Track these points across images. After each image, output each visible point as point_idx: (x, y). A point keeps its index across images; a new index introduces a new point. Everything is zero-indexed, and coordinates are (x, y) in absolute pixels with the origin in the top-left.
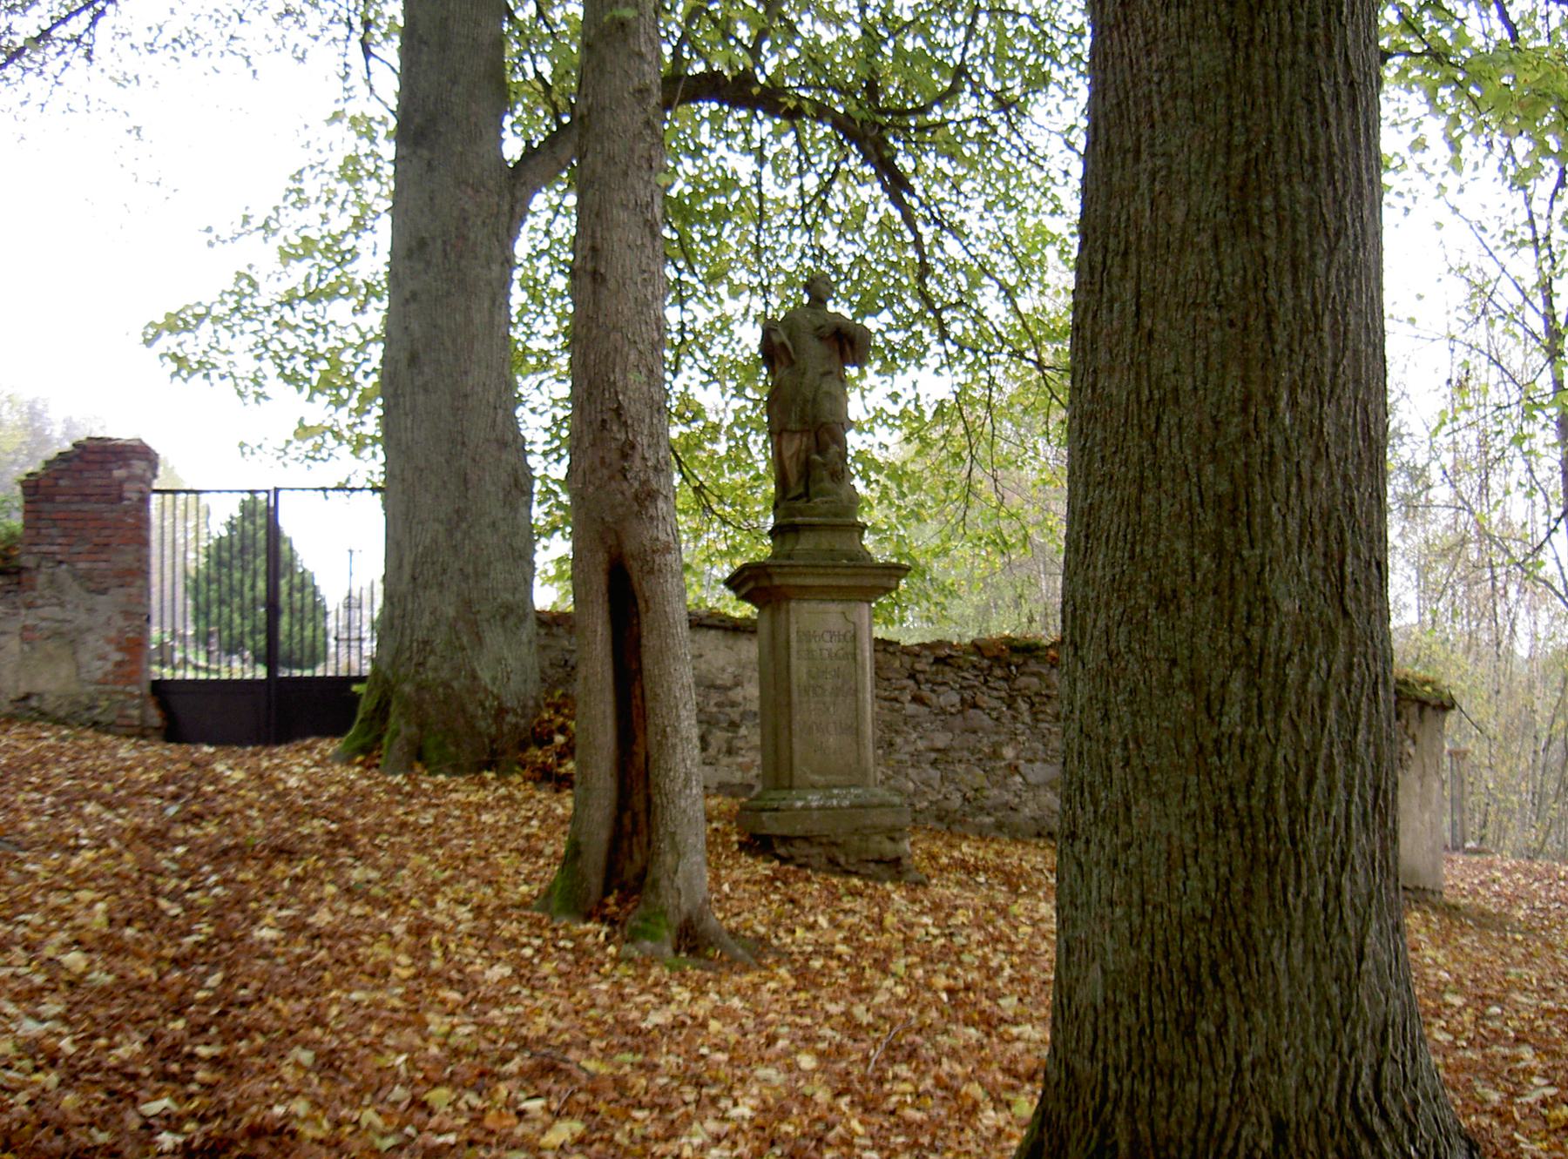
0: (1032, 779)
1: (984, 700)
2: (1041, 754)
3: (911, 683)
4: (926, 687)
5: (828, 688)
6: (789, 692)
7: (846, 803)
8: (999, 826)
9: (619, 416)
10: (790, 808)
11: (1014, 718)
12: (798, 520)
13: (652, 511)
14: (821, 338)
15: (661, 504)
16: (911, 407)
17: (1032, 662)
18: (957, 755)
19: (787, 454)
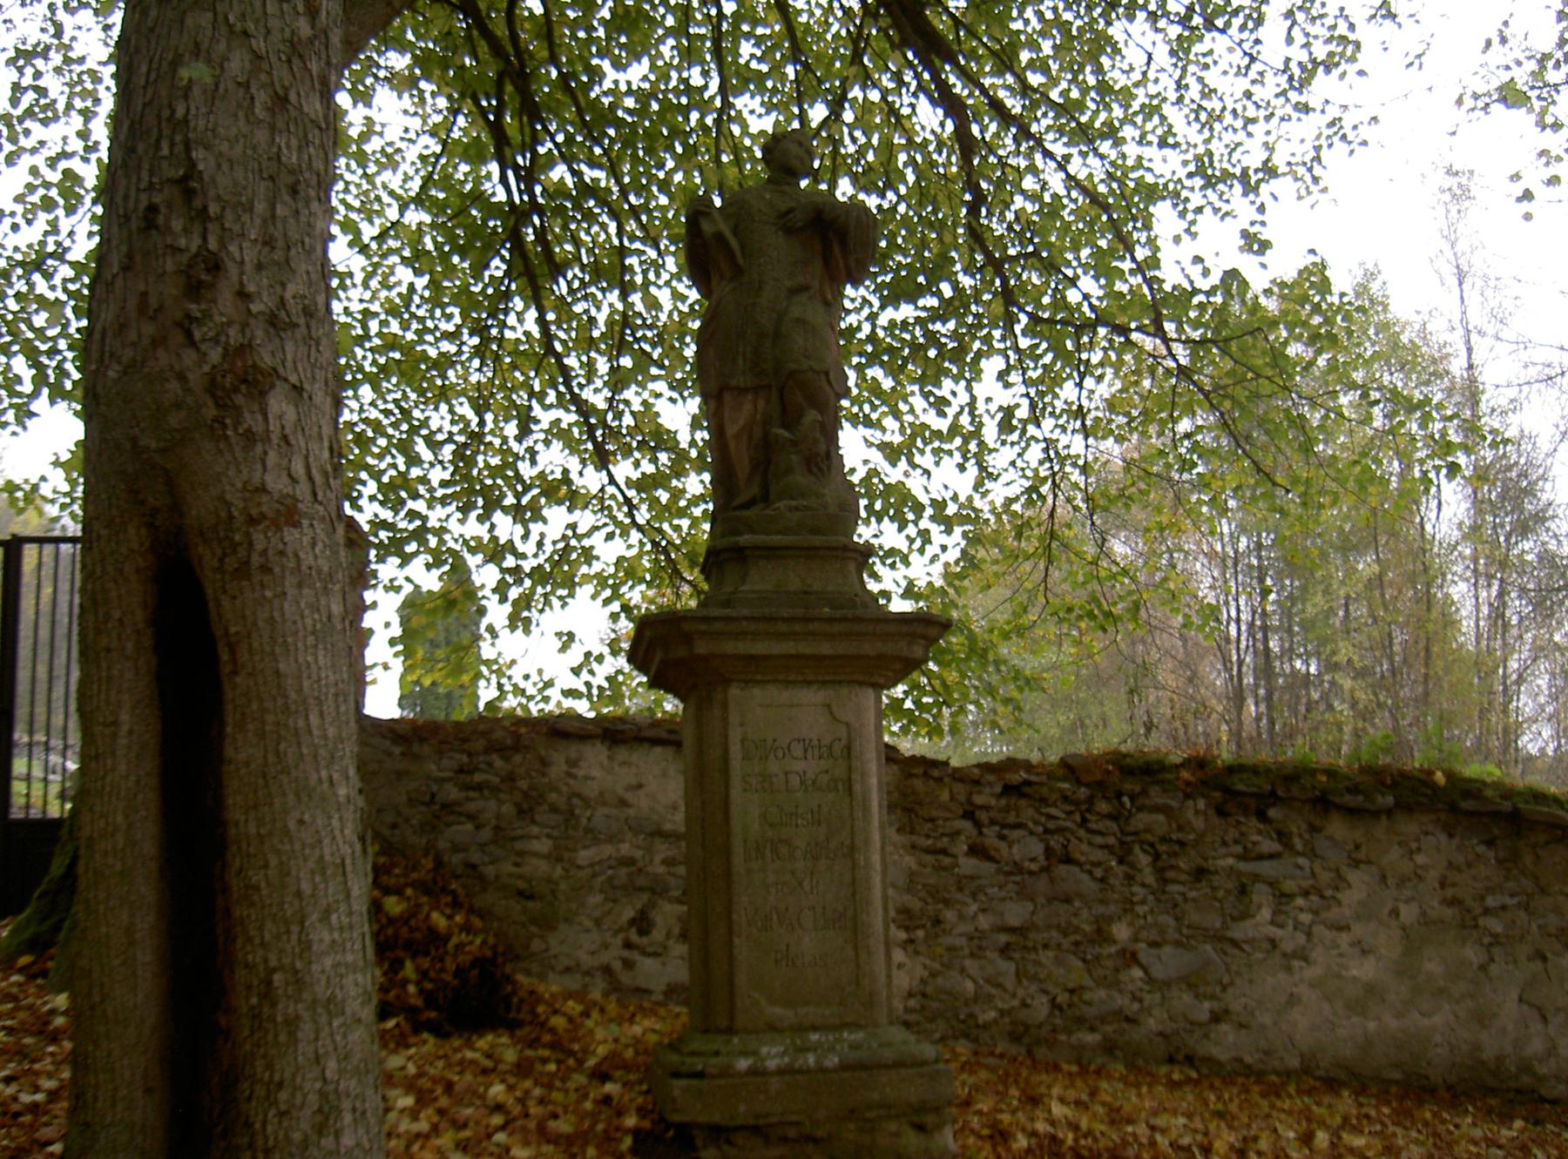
0: (1158, 972)
1: (1082, 850)
2: (1172, 934)
3: (967, 825)
4: (990, 831)
6: (727, 853)
7: (832, 1061)
8: (1109, 1048)
9: (189, 194)
10: (727, 1072)
11: (1130, 878)
12: (745, 539)
13: (252, 420)
14: (789, 231)
15: (279, 404)
16: (965, 420)
17: (1154, 791)
18: (1041, 937)
19: (731, 430)
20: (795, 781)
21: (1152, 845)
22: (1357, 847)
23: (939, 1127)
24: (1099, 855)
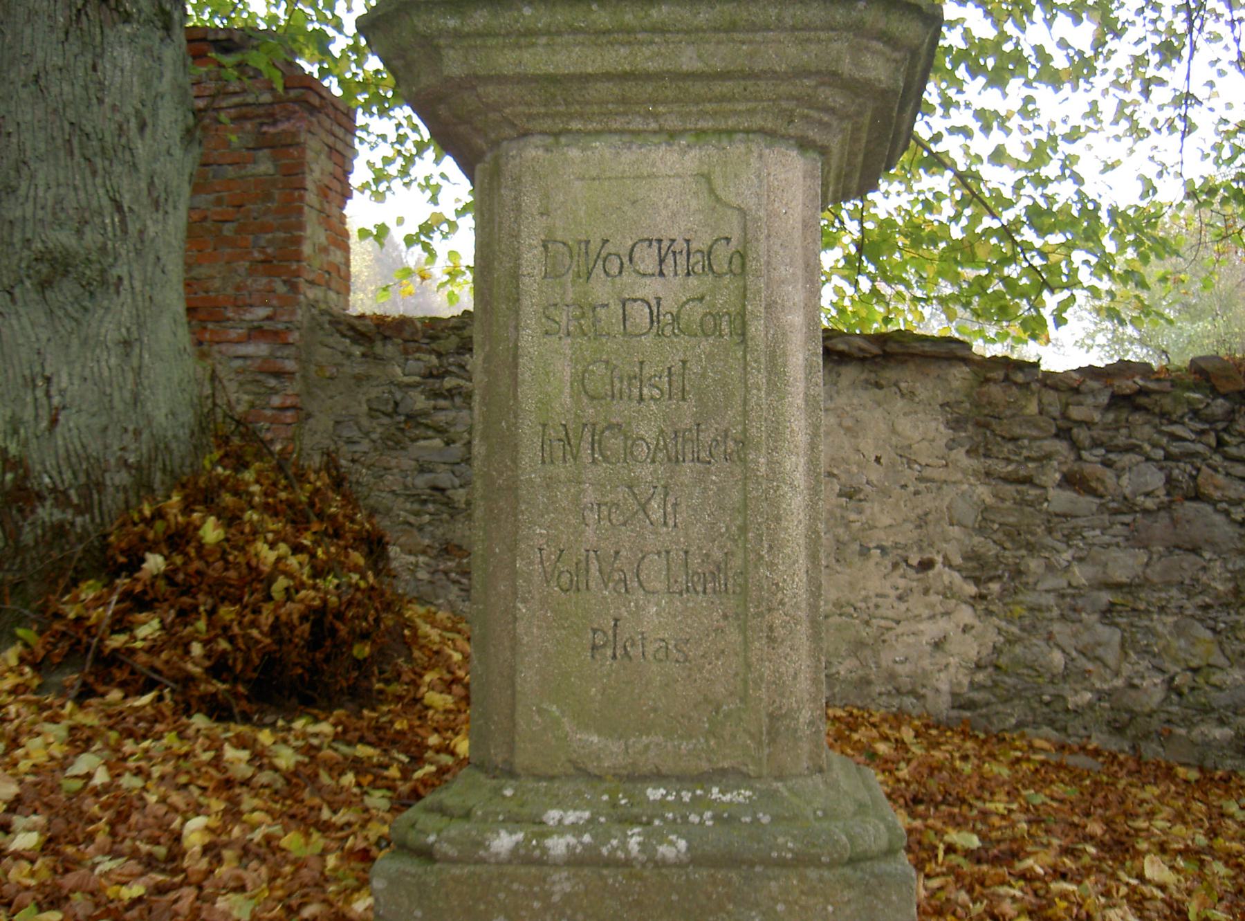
3: (1061, 446)
4: (1092, 457)
5: (647, 431)
7: (675, 848)
20: (640, 315)
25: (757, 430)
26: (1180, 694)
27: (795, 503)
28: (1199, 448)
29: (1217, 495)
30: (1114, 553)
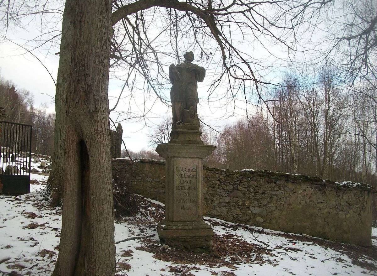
3: (218, 182)
15: (99, 115)
19: (176, 109)
20: (186, 175)
21: (254, 187)
22: (294, 190)
23: (210, 241)
24: (244, 189)
25: (197, 187)
26: (235, 218)
27: (200, 194)
28: (238, 183)
29: (240, 190)
30: (226, 198)
